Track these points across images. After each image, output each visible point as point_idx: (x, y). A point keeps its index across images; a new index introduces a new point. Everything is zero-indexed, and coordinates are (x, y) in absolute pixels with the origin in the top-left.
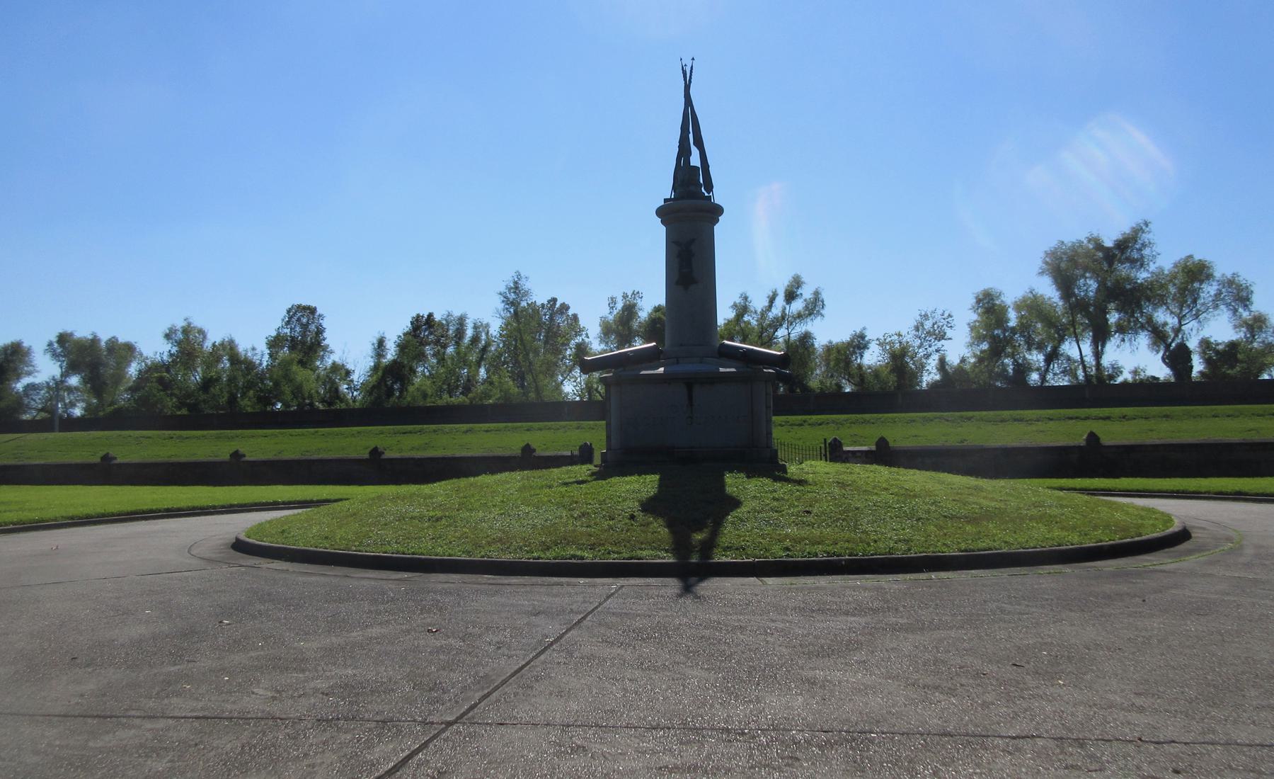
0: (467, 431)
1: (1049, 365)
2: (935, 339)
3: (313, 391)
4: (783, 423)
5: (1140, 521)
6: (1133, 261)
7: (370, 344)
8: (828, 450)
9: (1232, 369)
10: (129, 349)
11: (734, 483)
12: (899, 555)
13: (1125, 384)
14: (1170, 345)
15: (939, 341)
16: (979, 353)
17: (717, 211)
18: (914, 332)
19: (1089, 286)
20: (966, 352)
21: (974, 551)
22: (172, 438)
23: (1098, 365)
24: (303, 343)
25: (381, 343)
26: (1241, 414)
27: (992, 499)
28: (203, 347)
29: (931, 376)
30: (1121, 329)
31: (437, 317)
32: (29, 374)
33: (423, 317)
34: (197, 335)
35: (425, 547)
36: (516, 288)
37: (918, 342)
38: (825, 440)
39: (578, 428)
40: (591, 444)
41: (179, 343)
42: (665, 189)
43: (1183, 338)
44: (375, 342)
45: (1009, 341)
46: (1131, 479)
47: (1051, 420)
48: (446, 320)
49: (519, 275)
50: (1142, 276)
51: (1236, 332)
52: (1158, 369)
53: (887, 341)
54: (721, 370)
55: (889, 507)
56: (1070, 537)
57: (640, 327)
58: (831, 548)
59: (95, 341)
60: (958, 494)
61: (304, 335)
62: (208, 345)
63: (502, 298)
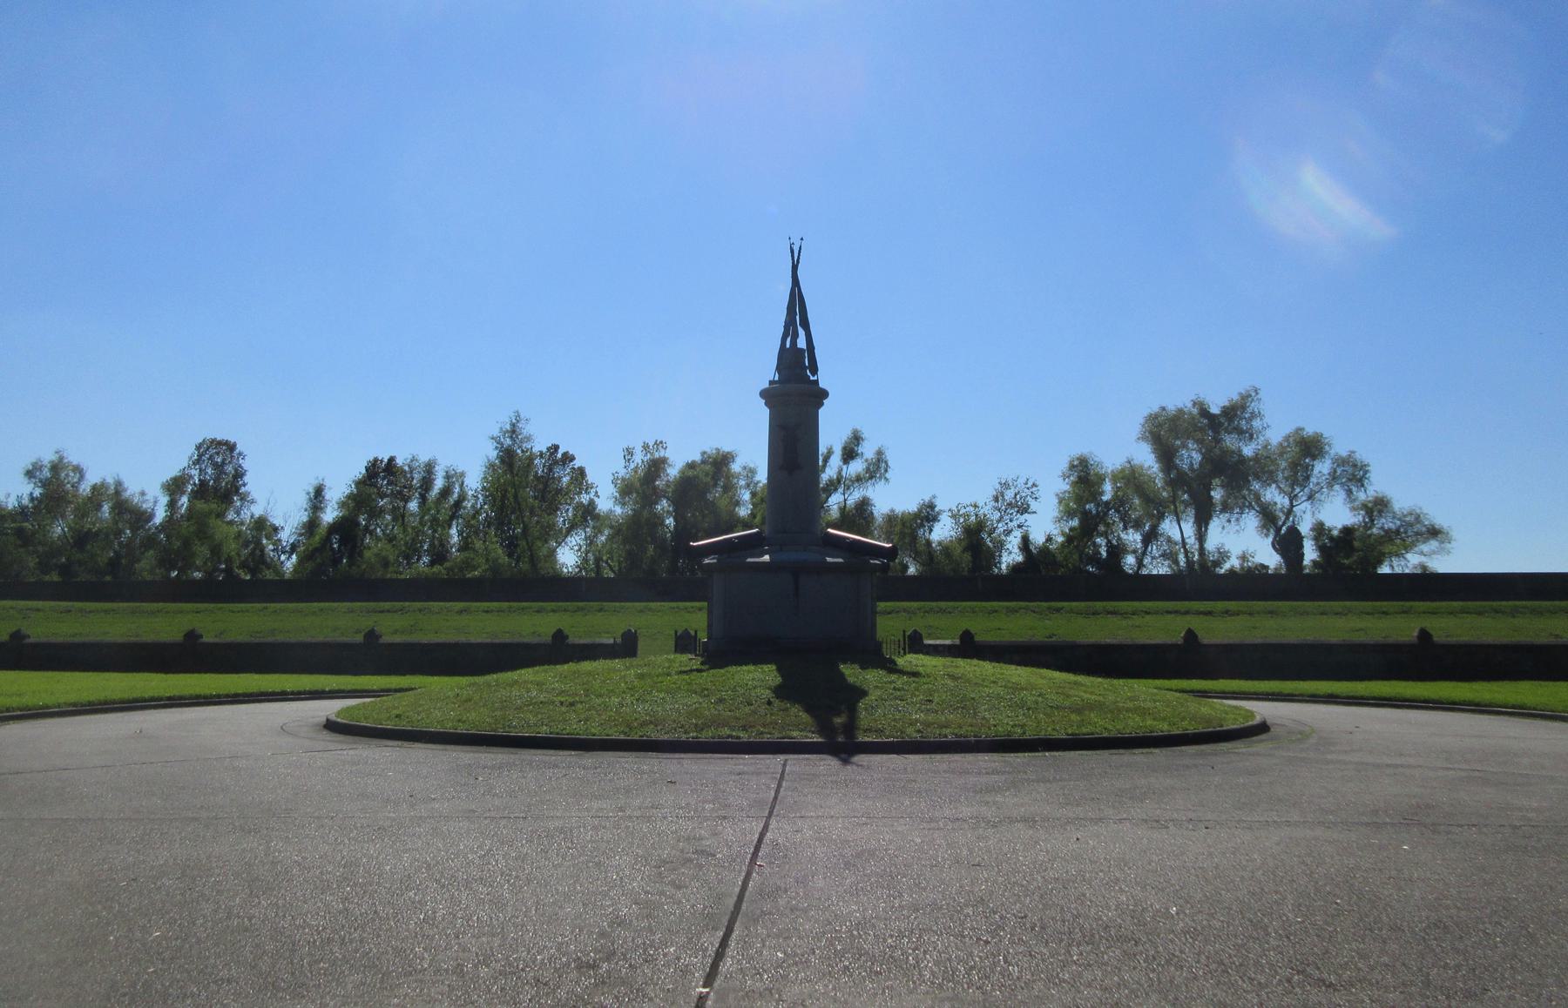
1: (1146, 548)
2: (1018, 512)
5: (1224, 715)
6: (1240, 432)
7: (304, 492)
9: (1347, 559)
11: (851, 672)
12: (1016, 737)
13: (1232, 571)
14: (1281, 529)
15: (1022, 514)
16: (1067, 531)
18: (993, 503)
19: (1191, 456)
22: (70, 611)
24: (216, 489)
25: (319, 492)
26: (1350, 612)
27: (1092, 693)
28: (78, 491)
29: (1011, 556)
30: (1226, 508)
31: (399, 461)
33: (382, 461)
35: (574, 727)
36: (513, 432)
37: (997, 515)
38: (904, 631)
39: (601, 610)
40: (636, 631)
41: (45, 484)
42: (767, 372)
43: (1293, 522)
44: (311, 490)
48: (409, 466)
49: (518, 416)
51: (1355, 515)
52: (1268, 557)
53: (961, 513)
55: (999, 697)
57: (668, 486)
61: (217, 479)
62: (85, 489)
63: (495, 444)
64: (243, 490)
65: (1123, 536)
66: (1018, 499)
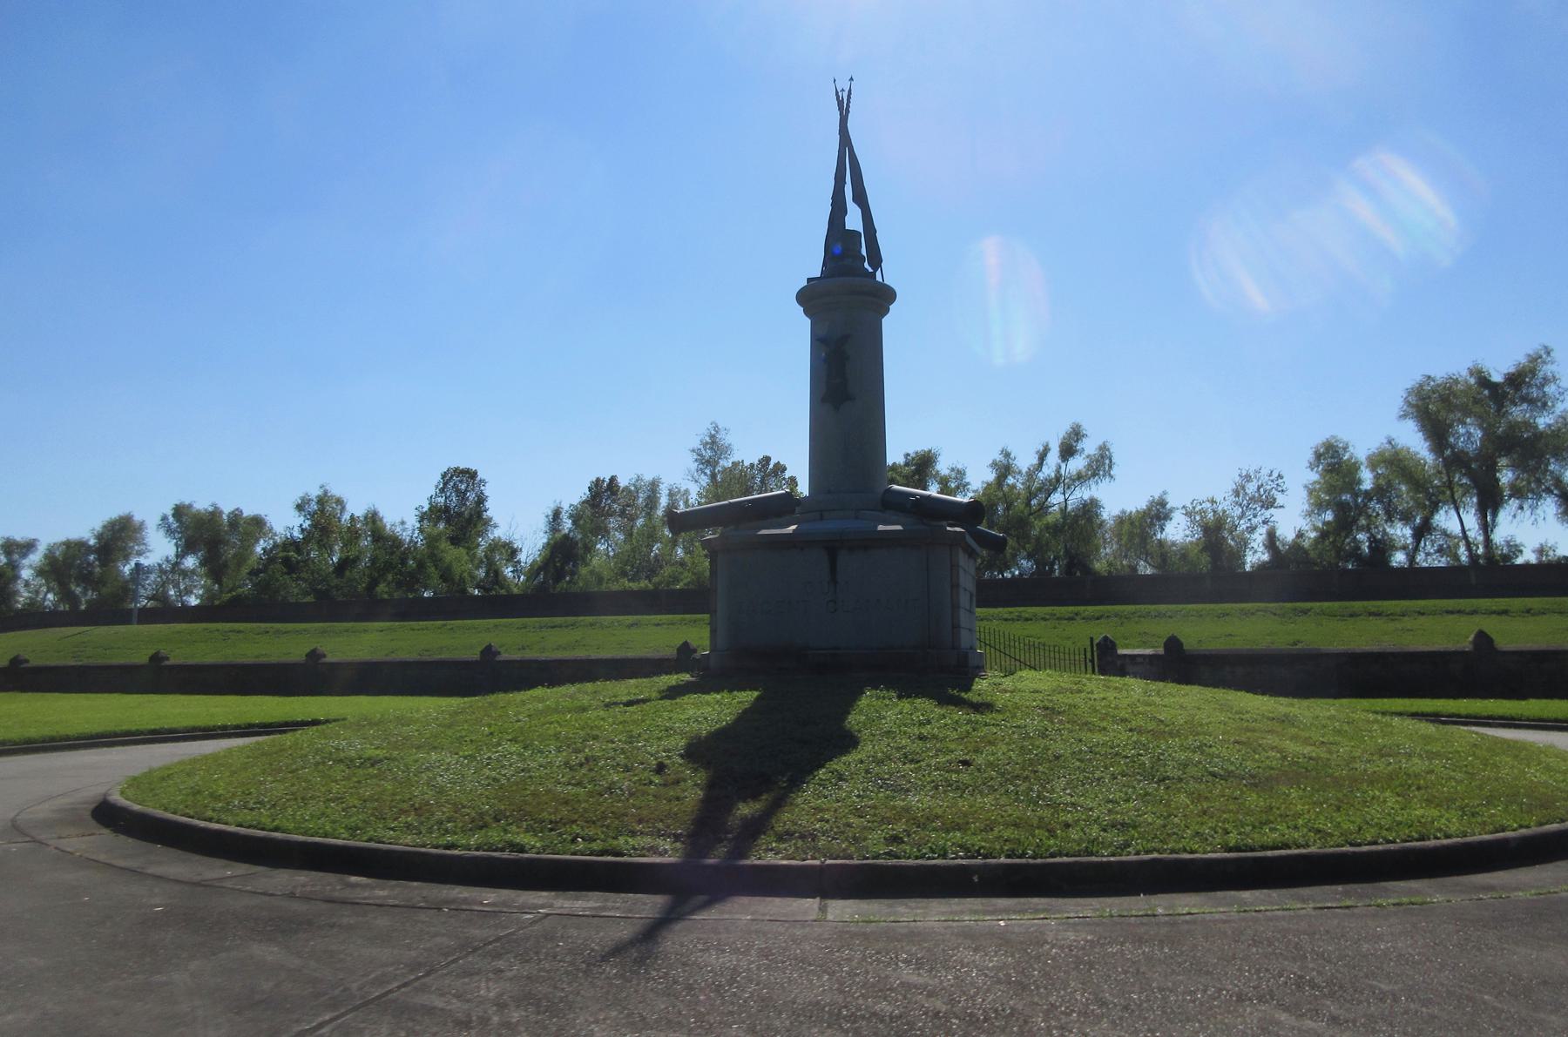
0: (632, 625)
1: (1418, 542)
2: (1262, 507)
3: (465, 574)
4: (1048, 617)
6: (1531, 401)
8: (1095, 654)
10: (258, 523)
12: (1105, 857)
13: (1527, 567)
15: (1267, 508)
16: (1320, 525)
17: (885, 296)
20: (1304, 524)
21: (1252, 850)
22: (268, 632)
23: (1488, 541)
25: (557, 514)
27: (1307, 741)
29: (1256, 555)
30: (1517, 492)
31: (623, 482)
32: (140, 554)
33: (603, 481)
34: (334, 505)
37: (1238, 511)
38: (1092, 639)
41: (312, 515)
42: (813, 265)
44: (550, 513)
45: (1362, 510)
46: (1544, 701)
47: (1423, 614)
48: (634, 485)
50: (1543, 421)
53: (1197, 509)
54: (881, 528)
56: (1443, 821)
58: (976, 839)
59: (215, 514)
60: (1248, 730)
63: (695, 457)
64: (485, 515)
65: (1390, 531)
66: (1262, 493)
